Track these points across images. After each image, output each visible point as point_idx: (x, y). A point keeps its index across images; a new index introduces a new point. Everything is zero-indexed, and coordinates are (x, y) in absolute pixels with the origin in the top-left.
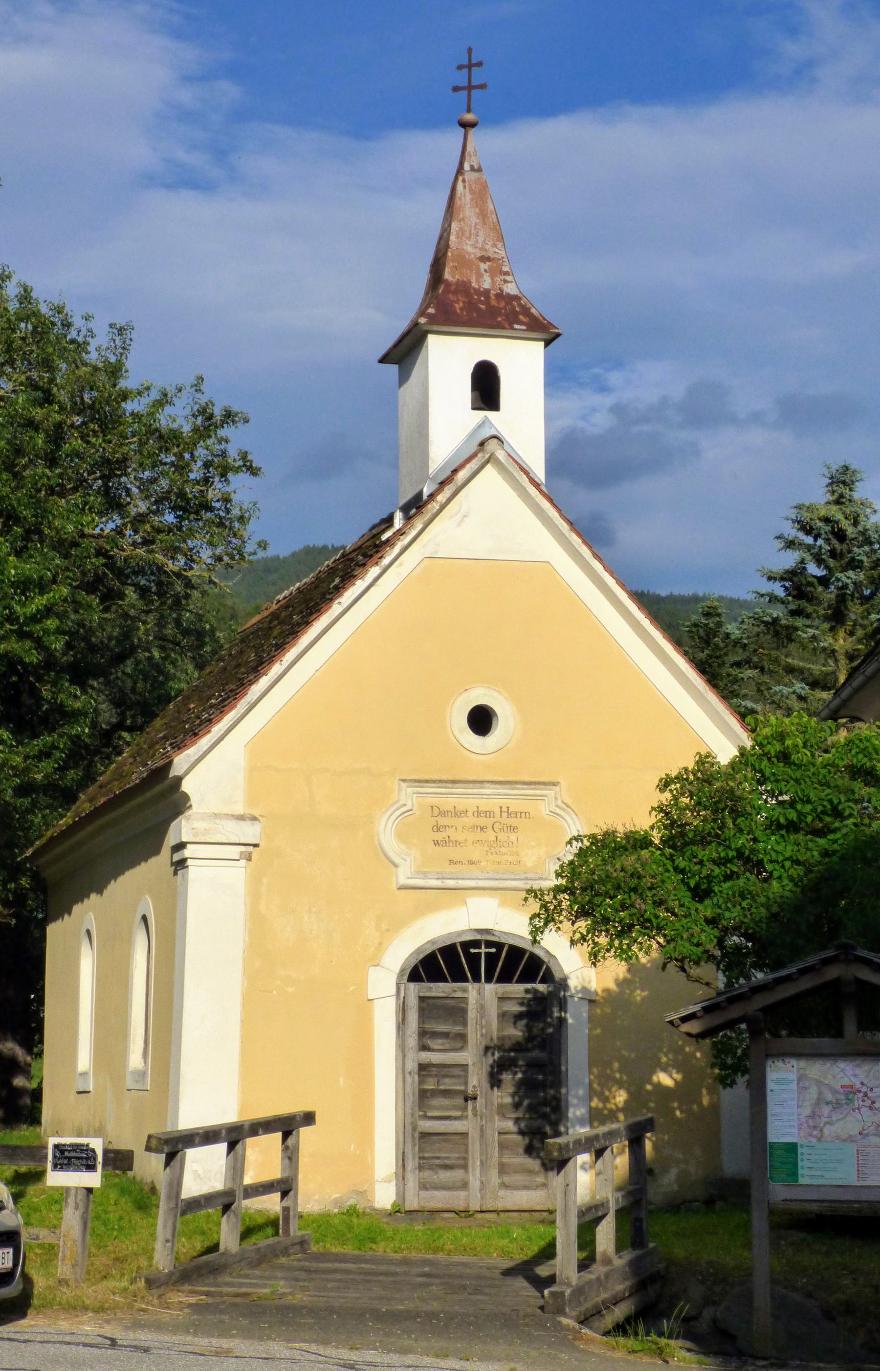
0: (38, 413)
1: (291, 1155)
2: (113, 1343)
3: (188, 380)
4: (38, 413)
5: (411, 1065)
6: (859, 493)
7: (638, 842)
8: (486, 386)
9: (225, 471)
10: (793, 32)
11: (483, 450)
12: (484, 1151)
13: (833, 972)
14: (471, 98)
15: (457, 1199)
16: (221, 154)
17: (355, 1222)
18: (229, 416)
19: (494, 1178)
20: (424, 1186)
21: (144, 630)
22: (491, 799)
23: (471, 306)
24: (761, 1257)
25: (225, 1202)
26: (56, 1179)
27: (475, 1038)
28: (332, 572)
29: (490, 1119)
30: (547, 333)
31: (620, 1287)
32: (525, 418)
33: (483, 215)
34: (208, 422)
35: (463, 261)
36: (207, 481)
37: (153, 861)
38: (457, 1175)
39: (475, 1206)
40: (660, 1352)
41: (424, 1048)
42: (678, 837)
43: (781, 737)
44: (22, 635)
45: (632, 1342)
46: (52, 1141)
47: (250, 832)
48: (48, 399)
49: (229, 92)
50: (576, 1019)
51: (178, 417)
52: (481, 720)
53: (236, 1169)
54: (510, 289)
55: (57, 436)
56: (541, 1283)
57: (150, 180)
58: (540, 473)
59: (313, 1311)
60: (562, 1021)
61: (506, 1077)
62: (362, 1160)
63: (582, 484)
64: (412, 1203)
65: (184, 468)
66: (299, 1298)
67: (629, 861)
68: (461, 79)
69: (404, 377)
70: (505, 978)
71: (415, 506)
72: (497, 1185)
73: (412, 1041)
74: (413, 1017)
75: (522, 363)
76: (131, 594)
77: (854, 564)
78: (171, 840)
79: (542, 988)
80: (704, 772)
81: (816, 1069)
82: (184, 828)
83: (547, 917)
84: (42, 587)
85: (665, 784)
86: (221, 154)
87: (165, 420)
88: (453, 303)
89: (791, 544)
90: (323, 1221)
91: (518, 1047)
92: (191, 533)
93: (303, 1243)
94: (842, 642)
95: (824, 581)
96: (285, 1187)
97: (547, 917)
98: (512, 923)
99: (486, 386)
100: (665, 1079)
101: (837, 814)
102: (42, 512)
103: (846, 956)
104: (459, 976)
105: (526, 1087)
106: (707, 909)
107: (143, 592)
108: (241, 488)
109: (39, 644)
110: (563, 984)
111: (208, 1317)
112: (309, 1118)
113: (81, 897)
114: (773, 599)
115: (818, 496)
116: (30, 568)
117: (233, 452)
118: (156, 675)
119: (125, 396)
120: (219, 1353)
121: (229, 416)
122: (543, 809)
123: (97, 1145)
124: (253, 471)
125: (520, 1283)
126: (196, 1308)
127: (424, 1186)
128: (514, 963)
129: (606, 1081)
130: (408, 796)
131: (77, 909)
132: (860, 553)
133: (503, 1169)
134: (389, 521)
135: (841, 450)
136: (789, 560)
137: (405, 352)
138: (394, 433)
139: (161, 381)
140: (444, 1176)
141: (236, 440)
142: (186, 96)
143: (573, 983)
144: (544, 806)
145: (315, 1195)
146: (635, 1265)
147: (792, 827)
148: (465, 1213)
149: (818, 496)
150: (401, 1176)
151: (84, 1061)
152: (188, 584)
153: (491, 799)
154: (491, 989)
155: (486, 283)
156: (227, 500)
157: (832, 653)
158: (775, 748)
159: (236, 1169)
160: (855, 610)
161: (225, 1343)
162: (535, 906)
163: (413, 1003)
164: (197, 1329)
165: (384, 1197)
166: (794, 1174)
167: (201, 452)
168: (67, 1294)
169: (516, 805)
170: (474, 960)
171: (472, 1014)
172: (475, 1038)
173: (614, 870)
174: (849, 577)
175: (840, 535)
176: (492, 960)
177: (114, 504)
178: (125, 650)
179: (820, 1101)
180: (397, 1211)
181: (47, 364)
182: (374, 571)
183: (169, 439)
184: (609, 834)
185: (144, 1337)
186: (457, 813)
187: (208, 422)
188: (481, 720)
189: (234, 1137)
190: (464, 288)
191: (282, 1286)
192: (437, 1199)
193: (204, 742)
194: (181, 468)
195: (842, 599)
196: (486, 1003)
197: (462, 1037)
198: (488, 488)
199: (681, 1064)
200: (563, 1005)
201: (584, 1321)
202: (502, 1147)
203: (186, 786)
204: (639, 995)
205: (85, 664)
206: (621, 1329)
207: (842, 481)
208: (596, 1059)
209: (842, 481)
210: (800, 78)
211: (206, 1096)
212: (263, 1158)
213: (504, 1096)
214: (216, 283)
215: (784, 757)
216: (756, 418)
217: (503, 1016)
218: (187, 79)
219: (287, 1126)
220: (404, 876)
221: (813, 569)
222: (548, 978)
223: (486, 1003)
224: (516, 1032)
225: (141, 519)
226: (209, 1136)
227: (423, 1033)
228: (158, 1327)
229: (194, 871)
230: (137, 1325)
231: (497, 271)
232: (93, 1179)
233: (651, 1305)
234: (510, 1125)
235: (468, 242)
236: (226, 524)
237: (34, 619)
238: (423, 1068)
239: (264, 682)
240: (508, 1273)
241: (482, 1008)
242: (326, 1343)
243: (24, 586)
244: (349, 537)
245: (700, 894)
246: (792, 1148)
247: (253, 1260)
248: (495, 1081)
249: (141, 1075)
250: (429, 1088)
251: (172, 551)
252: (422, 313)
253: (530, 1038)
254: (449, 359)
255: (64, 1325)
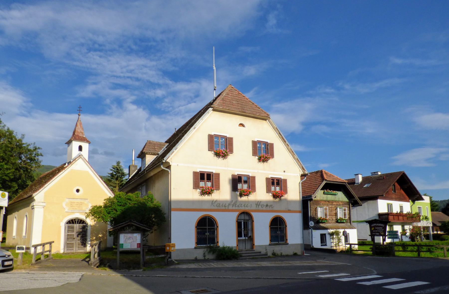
0: (9, 145)
1: (51, 247)
2: (28, 273)
3: (33, 143)
4: (9, 145)
5: (66, 234)
6: (120, 165)
7: (100, 207)
8: (80, 148)
9: (38, 156)
10: (110, 109)
11: (80, 156)
12: (76, 245)
13: (129, 223)
14: (79, 110)
15: (72, 251)
16: (29, 112)
17: (58, 255)
18: (39, 148)
19: (77, 249)
20: (67, 250)
21: (23, 176)
22: (79, 201)
23: (79, 138)
24: (118, 257)
25: (42, 253)
26: (17, 251)
27: (75, 231)
28: (56, 170)
29: (77, 241)
30: (89, 143)
31: (98, 261)
32: (85, 152)
33: (81, 127)
34: (35, 149)
35: (78, 132)
36: (35, 157)
37: (28, 208)
38: (72, 248)
39: (74, 252)
40: (105, 270)
41: (68, 232)
42: (106, 206)
43: (120, 195)
44: (6, 176)
45: (101, 268)
46: (17, 246)
47: (44, 204)
48: (11, 143)
49: (31, 105)
50: (89, 229)
51: (31, 148)
52: (78, 191)
53: (44, 249)
54: (84, 136)
55: (12, 149)
56: (88, 262)
57: (18, 115)
58: (87, 160)
59: (57, 267)
60: (87, 229)
61: (79, 236)
62: (59, 247)
63: (91, 162)
64: (66, 252)
65: (32, 155)
66: (54, 265)
67: (100, 209)
68: (79, 109)
69: (68, 146)
70: (80, 223)
71: (69, 163)
72: (78, 250)
73: (66, 231)
74: (67, 228)
75: (85, 146)
76: (22, 170)
77: (119, 173)
78: (32, 205)
79: (85, 225)
80: (109, 199)
81: (126, 235)
82: (34, 203)
83: (88, 216)
84: (10, 169)
85: (105, 200)
86: (29, 112)
87: (29, 148)
88: (76, 137)
89: (111, 170)
90: (53, 255)
91: (81, 232)
92: (32, 163)
93: (52, 258)
94: (117, 182)
95: (115, 175)
96: (50, 251)
97: (88, 216)
98: (83, 217)
99: (80, 148)
100: (100, 236)
101: (126, 204)
102: (9, 159)
103: (131, 221)
104: (73, 223)
105: (82, 237)
106: (109, 215)
107: (24, 171)
108: (40, 158)
109: (9, 177)
110: (87, 224)
111: (41, 269)
112: (53, 242)
113: (14, 212)
114: (109, 176)
115: (115, 164)
116: (8, 167)
117: (39, 153)
118: (24, 182)
119: (23, 144)
120: (45, 273)
121: (39, 148)
122: (86, 202)
123: (24, 247)
124: (42, 156)
125: (84, 262)
126: (39, 268)
127: (67, 250)
128: (81, 221)
129: (93, 236)
130: (67, 200)
131: (13, 214)
132: (120, 172)
133: (78, 247)
134: (65, 164)
135: (118, 160)
136: (111, 172)
137: (69, 143)
138: (65, 153)
139: (28, 143)
140: (70, 248)
141: (40, 151)
142: (24, 104)
143: (89, 224)
144: (86, 202)
145: (54, 251)
146: (99, 259)
147: (120, 205)
148: (73, 253)
149: (115, 164)
150: (64, 249)
151: (14, 234)
152: (31, 170)
153: (79, 201)
154: (78, 225)
155: (81, 135)
156: (38, 159)
157: (116, 183)
158: (119, 196)
159: (44, 249)
160: (119, 178)
161: (45, 272)
162: (86, 215)
163: (67, 227)
164: (40, 270)
165: (62, 251)
166: (123, 247)
167: (34, 153)
168: (19, 267)
169: (82, 202)
170: (75, 221)
171: (75, 228)
172: (75, 231)
173: (98, 210)
174: (119, 174)
175: (118, 169)
176: (78, 221)
177: (20, 158)
178: (20, 178)
179: (126, 239)
180: (64, 253)
181: (12, 139)
182: (64, 171)
183: (29, 150)
184: (96, 206)
185: (33, 272)
186: (74, 203)
187: (35, 149)
188: (78, 191)
189: (43, 245)
190: (78, 136)
191: (51, 264)
192: (69, 251)
193: (38, 192)
194: (31, 154)
195: (118, 177)
196: (77, 226)
197: (73, 231)
198: (80, 161)
199: (103, 234)
200: (87, 227)
201: (94, 266)
202: (78, 245)
203: (35, 198)
204: (97, 225)
205: (15, 180)
206: (97, 267)
207: (118, 163)
208: (92, 233)
209: (118, 163)
210: (111, 114)
211: (36, 240)
212: (47, 247)
213: (79, 238)
214: (34, 129)
215: (120, 197)
216: (101, 154)
217: (79, 228)
218: (25, 102)
219: (50, 243)
220: (66, 210)
221: (114, 173)
222: (85, 223)
223: (77, 226)
224: (81, 230)
225: (25, 161)
226: (40, 245)
227: (68, 231)
228: (34, 270)
229: (35, 209)
230: (31, 270)
231: (82, 134)
232: (24, 251)
233: (102, 263)
234: (79, 242)
235: (79, 129)
236: (37, 162)
237: (8, 174)
238: (68, 235)
239: (47, 184)
240: (82, 260)
241: (76, 227)
242: (60, 271)
243: (7, 169)
244: (58, 165)
245: (109, 213)
246: (123, 244)
247: (45, 261)
248: (78, 236)
249: (25, 237)
250: (68, 237)
251: (29, 166)
252: (72, 138)
253: (83, 231)
254: (75, 144)
255: (19, 271)
